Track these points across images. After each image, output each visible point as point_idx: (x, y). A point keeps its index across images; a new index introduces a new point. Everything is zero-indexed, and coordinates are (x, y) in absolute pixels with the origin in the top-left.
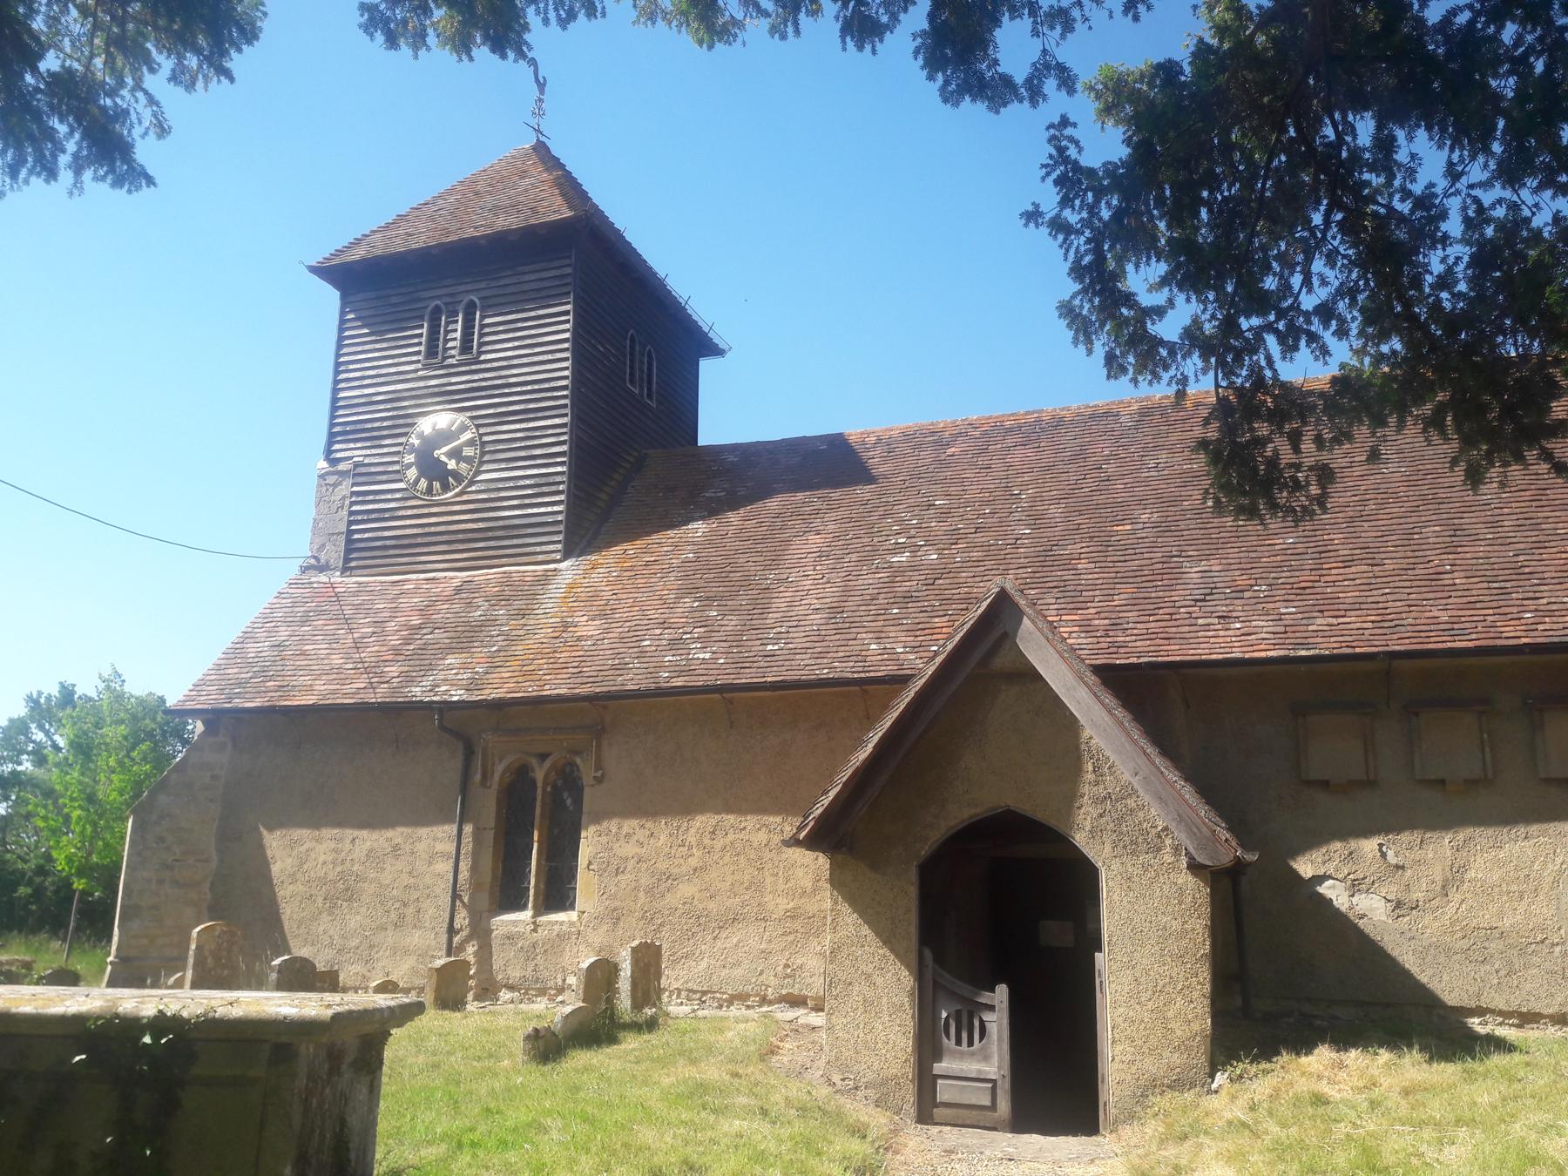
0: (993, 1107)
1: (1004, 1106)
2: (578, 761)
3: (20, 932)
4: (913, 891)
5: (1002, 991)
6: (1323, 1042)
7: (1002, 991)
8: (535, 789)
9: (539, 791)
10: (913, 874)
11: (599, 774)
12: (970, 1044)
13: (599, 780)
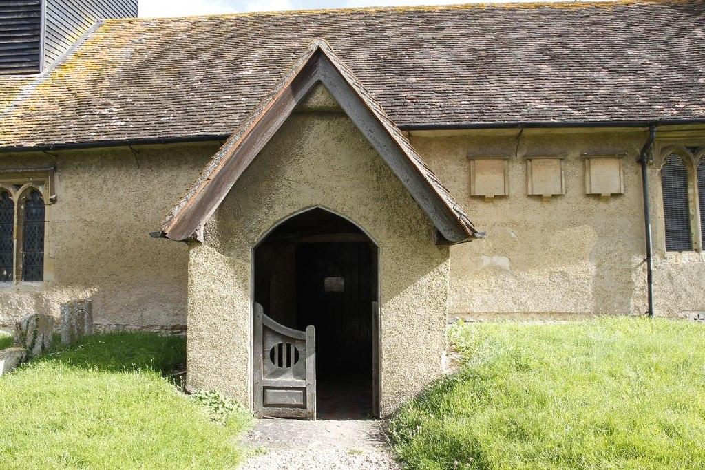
0: (304, 407)
1: (312, 406)
2: (41, 189)
3: (144, 369)
4: (249, 267)
5: (311, 331)
6: (324, 280)
7: (311, 331)
8: (13, 205)
9: (16, 208)
10: (250, 255)
11: (53, 197)
12: (289, 365)
13: (53, 201)
